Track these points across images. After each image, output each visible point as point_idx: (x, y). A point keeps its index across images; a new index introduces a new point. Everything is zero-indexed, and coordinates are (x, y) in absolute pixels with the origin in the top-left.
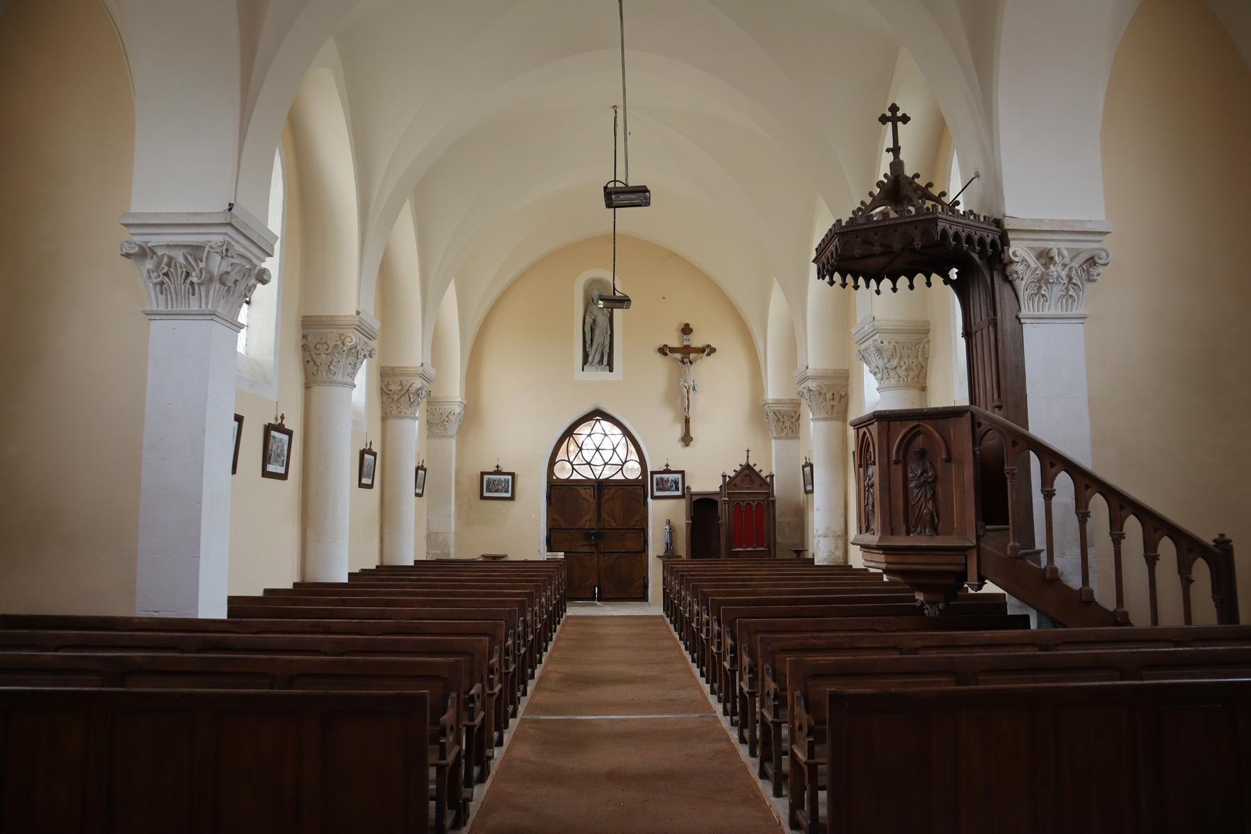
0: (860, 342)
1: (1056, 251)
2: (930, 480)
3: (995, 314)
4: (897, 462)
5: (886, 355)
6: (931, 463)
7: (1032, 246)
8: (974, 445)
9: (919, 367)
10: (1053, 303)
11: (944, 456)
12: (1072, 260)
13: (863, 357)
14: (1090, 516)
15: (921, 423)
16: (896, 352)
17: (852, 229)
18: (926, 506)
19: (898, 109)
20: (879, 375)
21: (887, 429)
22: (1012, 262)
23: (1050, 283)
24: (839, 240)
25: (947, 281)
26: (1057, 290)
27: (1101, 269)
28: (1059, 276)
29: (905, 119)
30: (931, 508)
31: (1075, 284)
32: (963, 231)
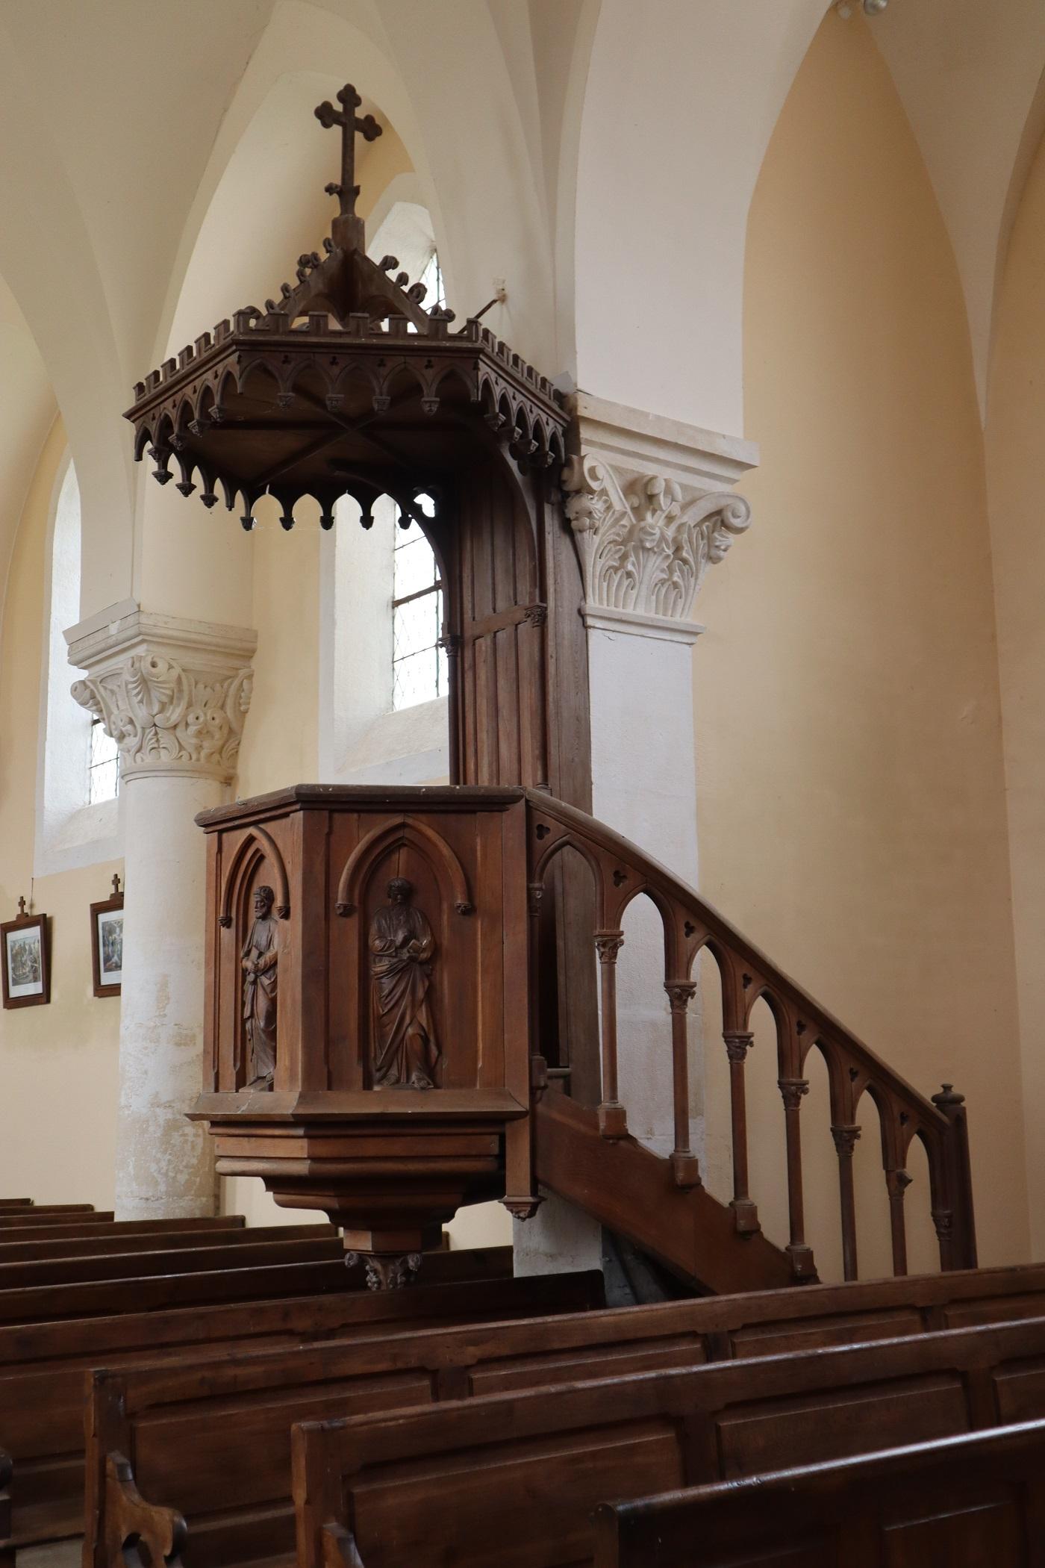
0: (84, 664)
1: (663, 483)
2: (424, 956)
3: (543, 597)
4: (347, 912)
5: (158, 695)
6: (425, 917)
7: (619, 464)
8: (530, 878)
9: (225, 730)
10: (644, 592)
11: (459, 901)
12: (684, 507)
13: (93, 697)
14: (751, 1044)
15: (410, 821)
16: (181, 691)
17: (276, 338)
18: (413, 1018)
20: (132, 742)
21: (326, 830)
22: (583, 489)
23: (644, 549)
24: (239, 362)
25: (410, 513)
26: (653, 568)
27: (732, 538)
28: (663, 538)
30: (424, 1024)
31: (685, 561)
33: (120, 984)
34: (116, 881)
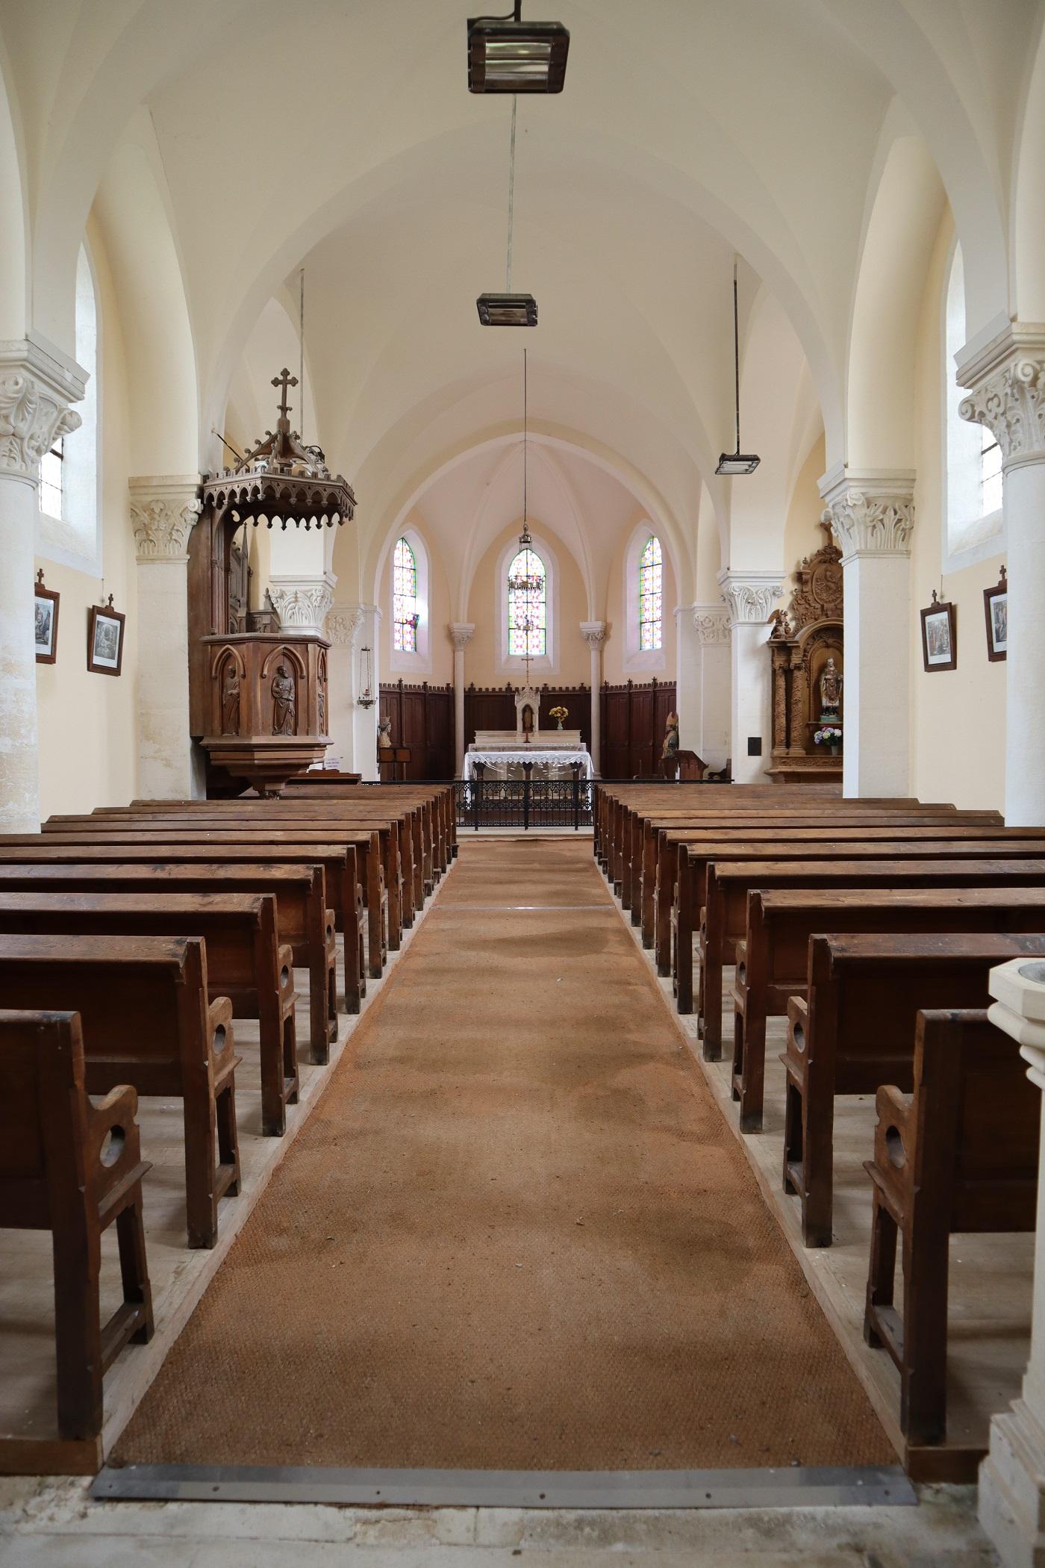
19: (289, 373)
29: (294, 382)
32: (325, 490)
33: (1005, 651)
34: (1003, 571)
